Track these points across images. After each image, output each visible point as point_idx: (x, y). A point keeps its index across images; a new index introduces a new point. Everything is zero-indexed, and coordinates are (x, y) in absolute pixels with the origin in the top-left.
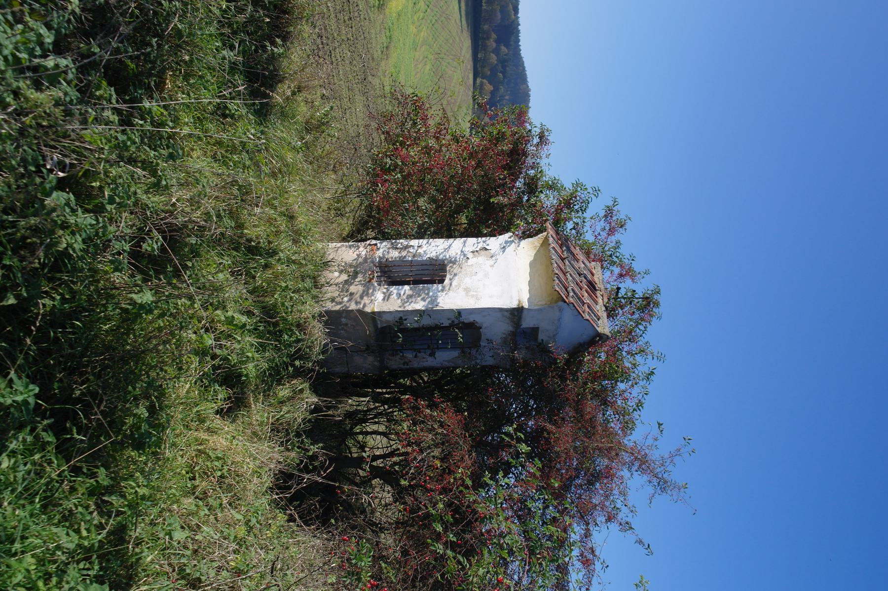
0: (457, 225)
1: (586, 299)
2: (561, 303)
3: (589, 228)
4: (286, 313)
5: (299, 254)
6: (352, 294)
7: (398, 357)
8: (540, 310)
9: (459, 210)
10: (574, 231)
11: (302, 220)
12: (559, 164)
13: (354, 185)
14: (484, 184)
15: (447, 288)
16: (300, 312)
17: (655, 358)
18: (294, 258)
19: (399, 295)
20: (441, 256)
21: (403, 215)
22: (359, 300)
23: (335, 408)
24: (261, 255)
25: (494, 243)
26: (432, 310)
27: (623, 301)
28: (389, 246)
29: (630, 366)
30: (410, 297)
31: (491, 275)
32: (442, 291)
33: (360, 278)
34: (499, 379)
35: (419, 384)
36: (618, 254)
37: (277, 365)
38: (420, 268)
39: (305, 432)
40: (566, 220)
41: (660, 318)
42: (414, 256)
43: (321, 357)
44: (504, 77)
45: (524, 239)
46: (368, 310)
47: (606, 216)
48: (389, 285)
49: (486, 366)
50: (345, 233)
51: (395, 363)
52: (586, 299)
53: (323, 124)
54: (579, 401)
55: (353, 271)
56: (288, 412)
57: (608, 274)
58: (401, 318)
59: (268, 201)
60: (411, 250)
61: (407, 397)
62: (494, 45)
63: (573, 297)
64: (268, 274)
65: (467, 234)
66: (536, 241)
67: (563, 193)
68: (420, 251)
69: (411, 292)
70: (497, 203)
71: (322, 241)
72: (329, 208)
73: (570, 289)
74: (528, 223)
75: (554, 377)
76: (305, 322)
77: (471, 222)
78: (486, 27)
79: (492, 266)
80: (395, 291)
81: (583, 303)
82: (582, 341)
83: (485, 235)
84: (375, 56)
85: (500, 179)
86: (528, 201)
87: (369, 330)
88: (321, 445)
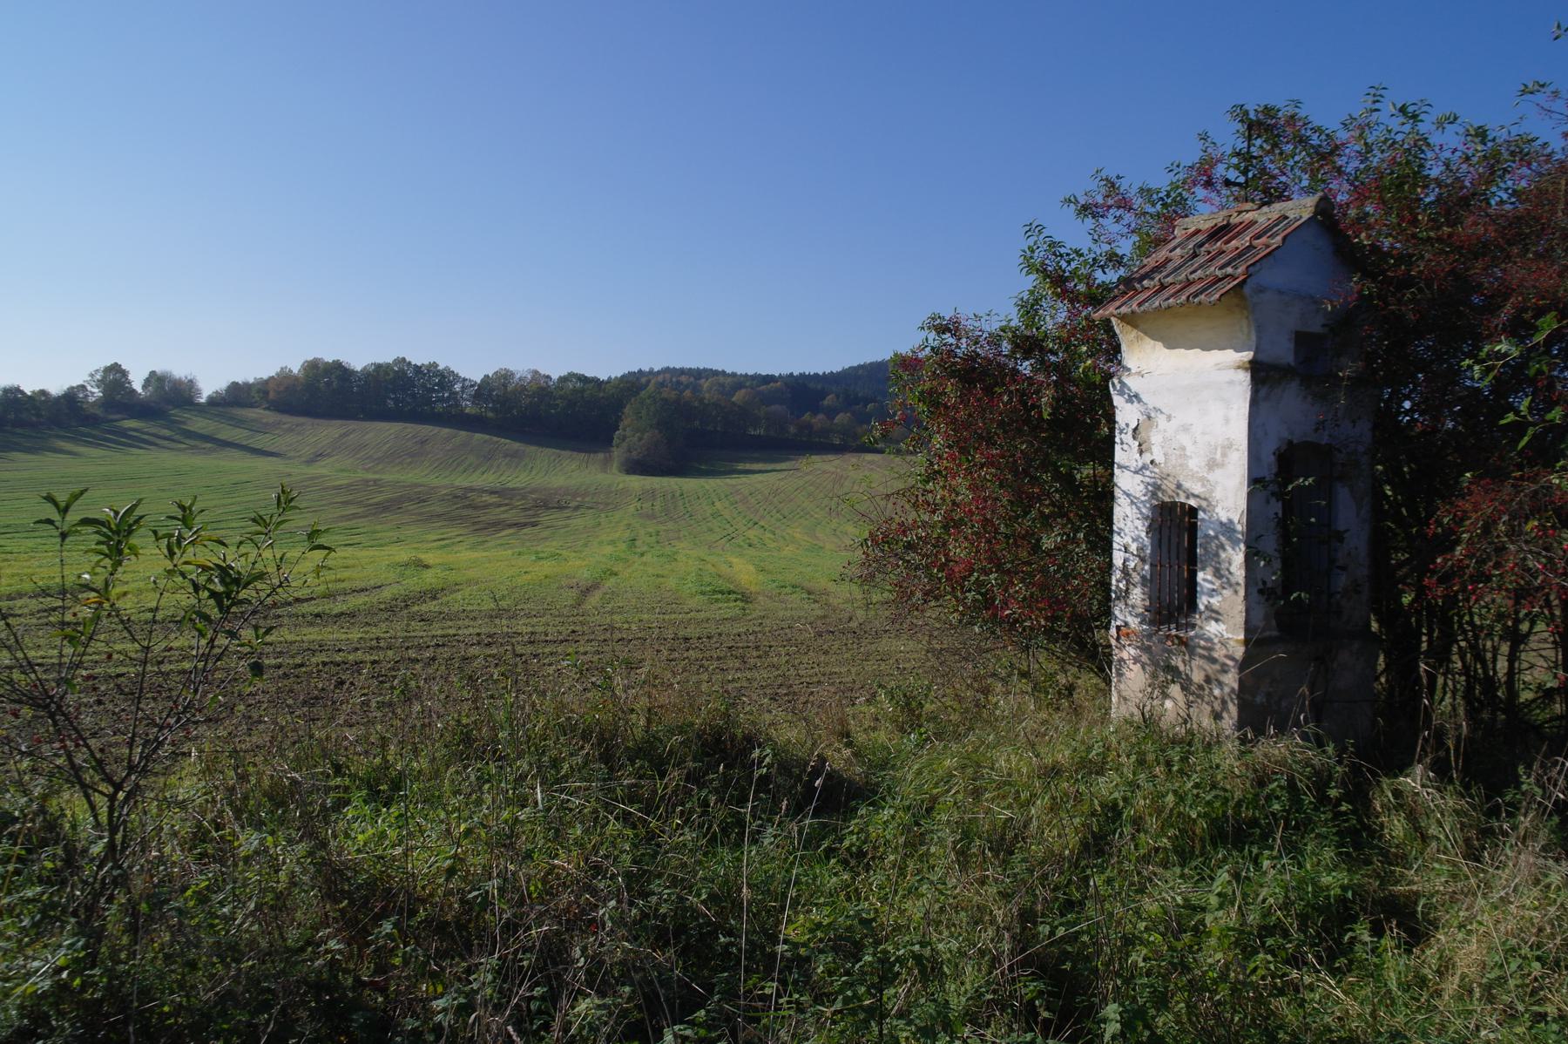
2: (1247, 290)
6: (1208, 680)
8: (1260, 330)
11: (1063, 756)
12: (991, 298)
17: (1377, 106)
25: (1126, 414)
30: (1218, 573)
31: (1188, 418)
33: (1177, 661)
39: (1489, 798)
41: (1297, 104)
44: (873, 400)
46: (1239, 652)
53: (908, 704)
55: (1165, 673)
60: (1132, 565)
62: (821, 416)
63: (1236, 268)
68: (1133, 547)
69: (1209, 570)
73: (1219, 273)
78: (792, 429)
79: (1169, 418)
81: (1251, 247)
83: (1112, 430)
84: (820, 613)
88: (1521, 769)
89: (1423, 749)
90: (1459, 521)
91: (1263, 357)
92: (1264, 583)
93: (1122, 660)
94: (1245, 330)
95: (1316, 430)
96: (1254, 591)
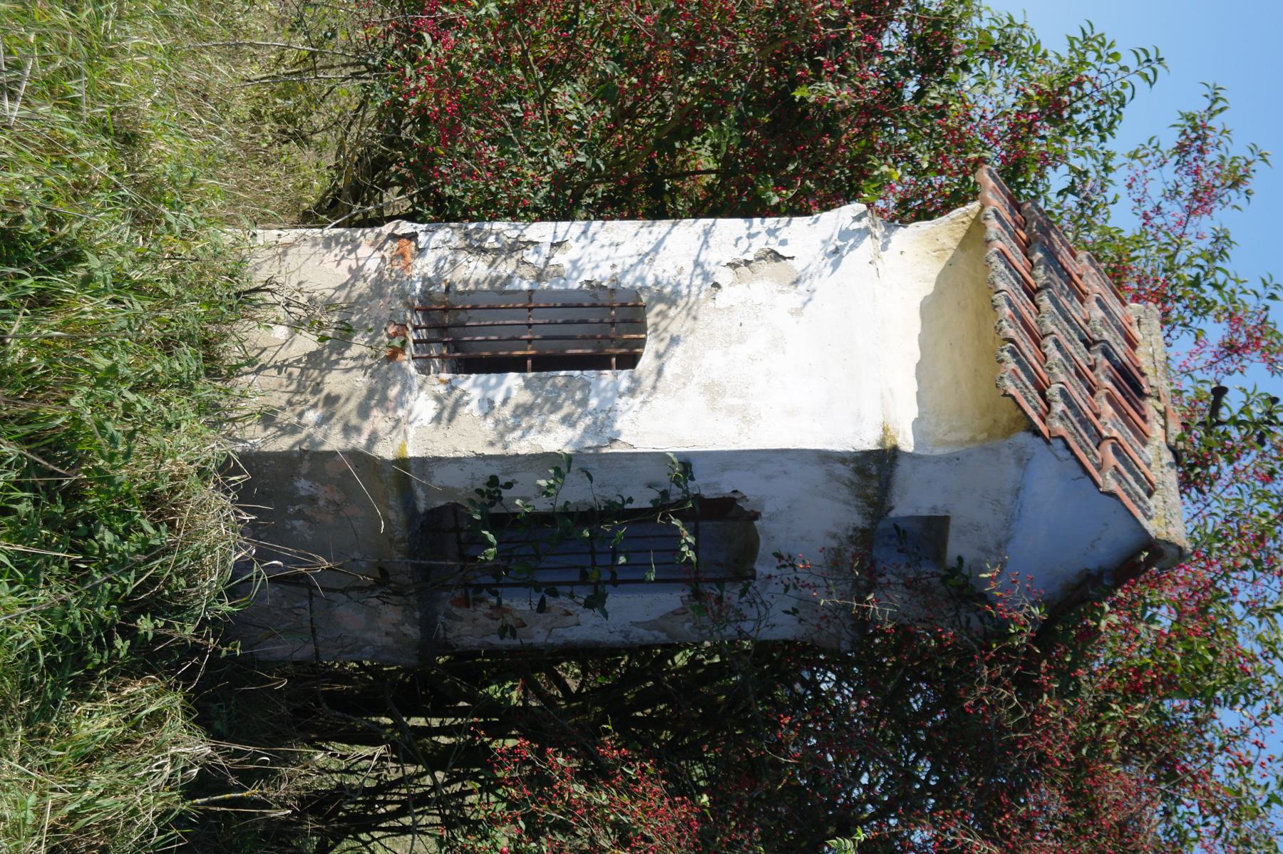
0: (682, 176)
1: (1110, 423)
2: (1023, 438)
3: (1121, 189)
4: (111, 458)
5: (156, 261)
6: (331, 400)
7: (483, 609)
8: (953, 460)
9: (688, 125)
10: (1071, 201)
11: (164, 151)
13: (342, 37)
14: (774, 39)
15: (647, 383)
16: (159, 455)
18: (136, 275)
19: (488, 406)
20: (628, 281)
21: (501, 141)
22: (354, 421)
23: (266, 775)
24: (23, 262)
25: (805, 235)
26: (598, 457)
27: (1235, 433)
28: (457, 241)
29: (1258, 650)
30: (524, 411)
32: (631, 392)
33: (359, 345)
34: (813, 685)
35: (549, 701)
36: (1220, 277)
37: (74, 631)
38: (560, 315)
40: (1045, 160)
42: (539, 277)
43: (226, 607)
45: (904, 223)
46: (385, 451)
47: (1181, 149)
48: (455, 371)
49: (774, 645)
50: (310, 199)
51: (471, 628)
52: (1110, 423)
54: (1080, 765)
55: (337, 326)
56: (110, 790)
57: (1184, 342)
58: (495, 478)
59: (50, 83)
61: (510, 743)
64: (50, 326)
65: (714, 205)
66: (944, 231)
67: (1037, 71)
68: (560, 258)
70: (817, 105)
71: (230, 221)
72: (256, 112)
73: (1053, 390)
74: (917, 172)
75: (996, 682)
76: (173, 491)
77: (727, 168)
79: (797, 312)
80: (476, 394)
81: (1099, 439)
82: (1092, 565)
83: (775, 212)
85: (827, 22)
86: (919, 96)
87: (385, 517)
89: (238, 753)
90: (628, 787)
91: (903, 468)
92: (509, 485)
93: (356, 246)
94: (952, 437)
95: (779, 556)
96: (494, 471)
